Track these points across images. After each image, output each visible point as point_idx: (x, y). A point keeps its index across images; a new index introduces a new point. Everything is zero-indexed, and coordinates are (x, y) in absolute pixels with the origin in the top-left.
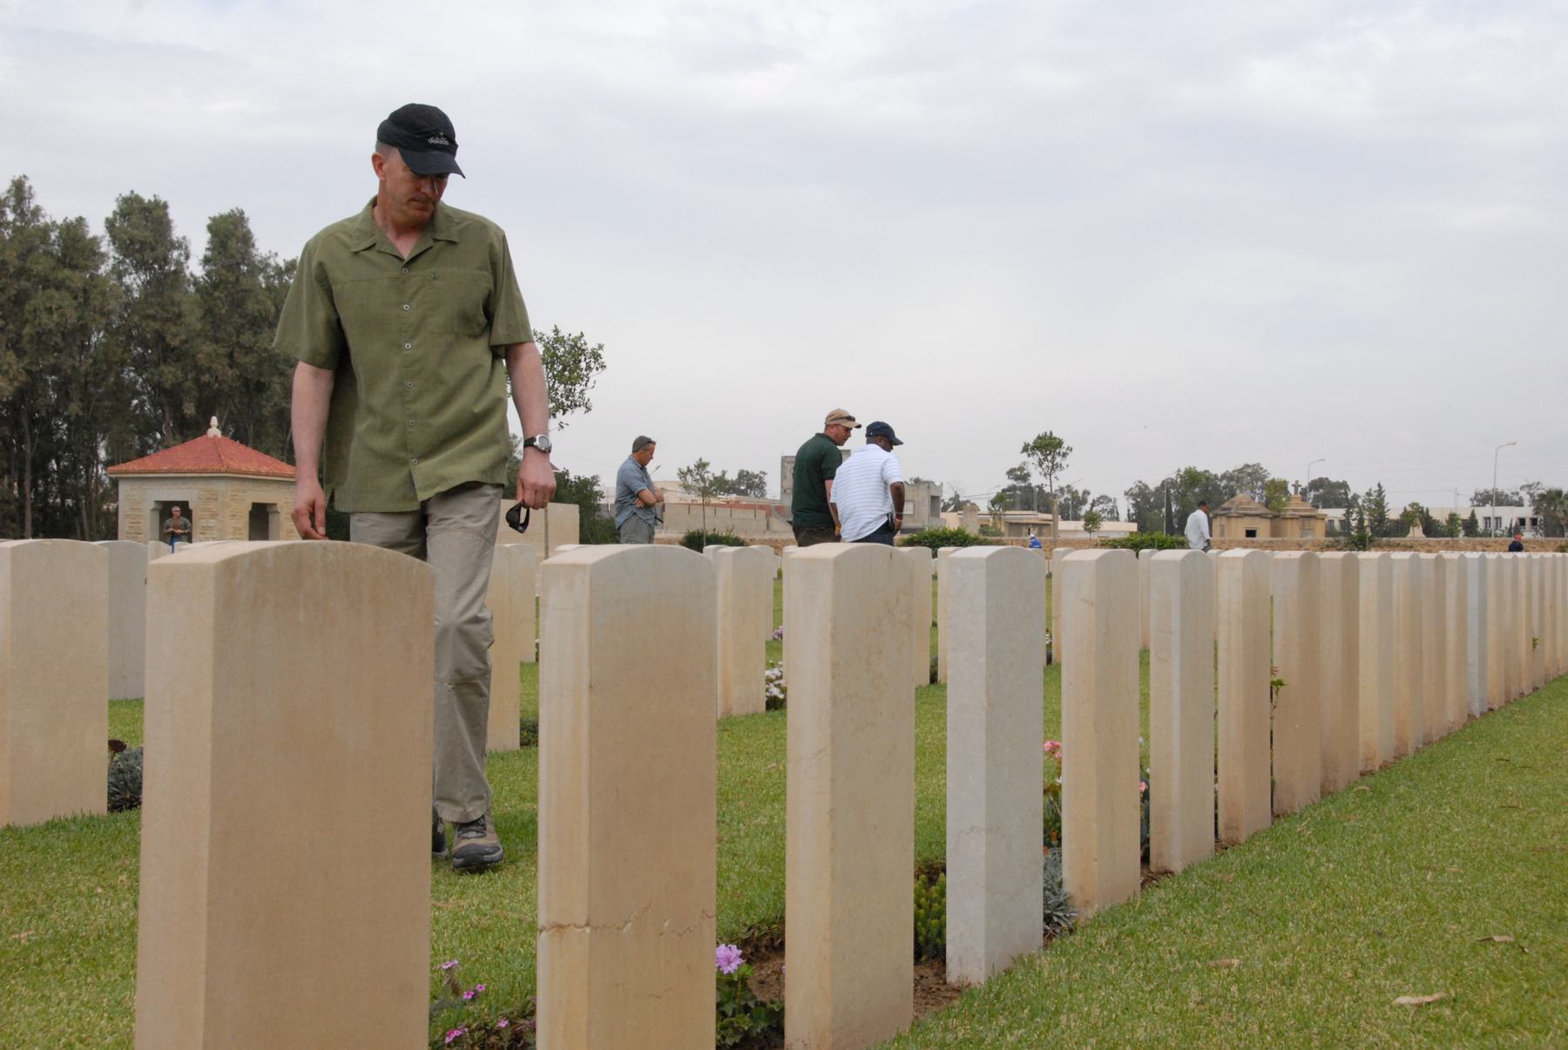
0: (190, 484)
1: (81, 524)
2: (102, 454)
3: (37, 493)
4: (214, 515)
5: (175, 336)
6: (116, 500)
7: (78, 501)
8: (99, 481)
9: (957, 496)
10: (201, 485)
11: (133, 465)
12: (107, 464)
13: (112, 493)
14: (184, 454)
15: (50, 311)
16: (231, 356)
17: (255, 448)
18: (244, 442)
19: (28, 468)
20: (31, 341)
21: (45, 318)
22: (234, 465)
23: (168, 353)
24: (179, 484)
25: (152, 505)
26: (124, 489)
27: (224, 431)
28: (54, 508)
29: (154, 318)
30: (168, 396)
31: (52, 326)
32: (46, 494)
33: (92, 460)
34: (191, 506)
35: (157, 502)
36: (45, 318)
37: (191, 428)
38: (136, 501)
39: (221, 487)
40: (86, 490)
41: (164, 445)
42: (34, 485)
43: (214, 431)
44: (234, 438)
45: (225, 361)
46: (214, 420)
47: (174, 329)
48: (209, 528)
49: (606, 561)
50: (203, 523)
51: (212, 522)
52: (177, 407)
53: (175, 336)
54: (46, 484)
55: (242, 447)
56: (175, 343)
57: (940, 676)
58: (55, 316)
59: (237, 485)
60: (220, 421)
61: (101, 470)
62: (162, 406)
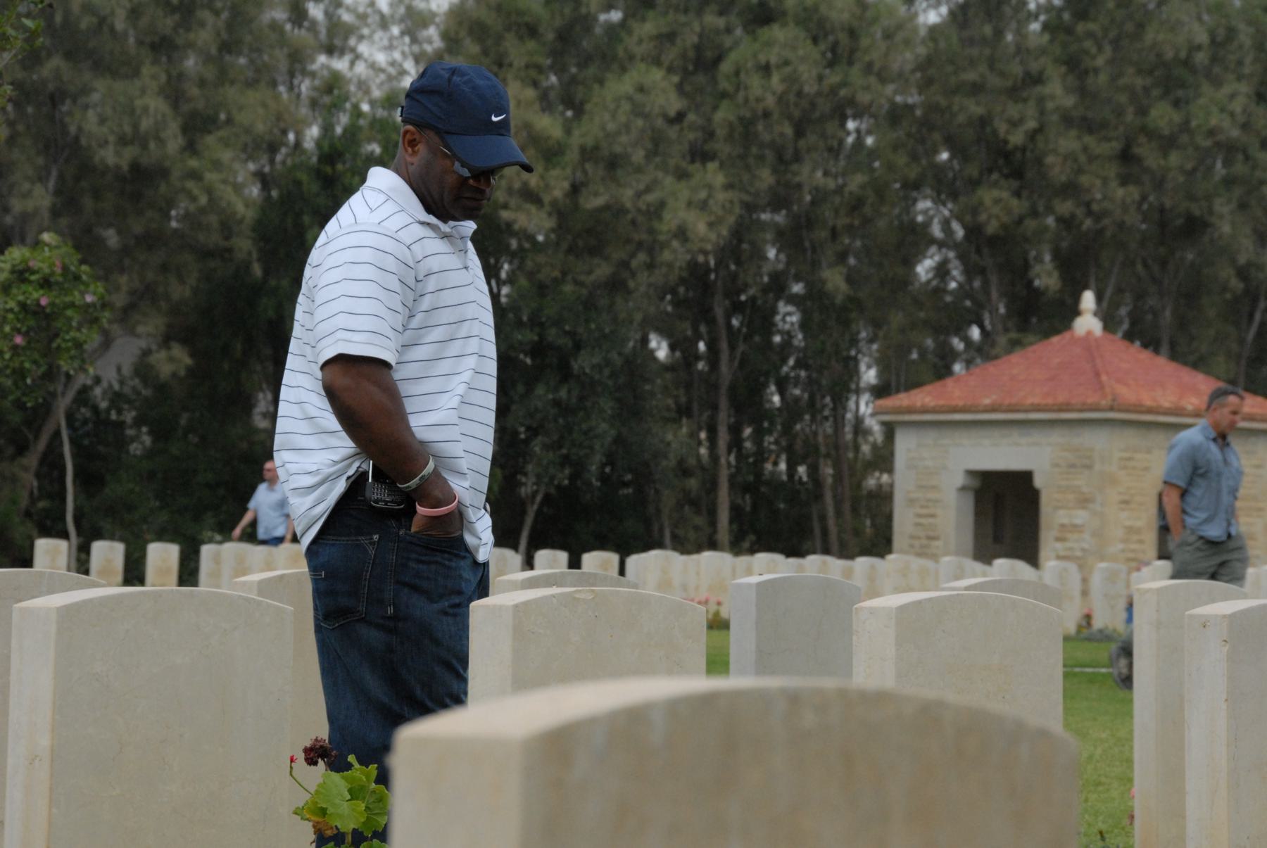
0: (1037, 436)
1: (823, 518)
2: (870, 375)
3: (740, 457)
4: (1084, 501)
5: (1014, 124)
6: (890, 470)
7: (814, 470)
8: (859, 428)
9: (314, 754)
10: (1057, 437)
11: (922, 397)
12: (880, 391)
13: (884, 459)
14: (1028, 371)
15: (766, 69)
16: (1126, 156)
17: (1175, 356)
18: (1152, 344)
19: (724, 403)
20: (730, 138)
21: (755, 83)
22: (1128, 394)
23: (1014, 165)
24: (1015, 435)
25: (960, 480)
26: (905, 445)
27: (1109, 322)
28: (775, 484)
29: (976, 89)
30: (992, 251)
31: (770, 101)
32: (761, 456)
33: (844, 386)
34: (1038, 482)
35: (971, 473)
36: (755, 83)
37: (1042, 316)
38: (931, 472)
39: (1097, 441)
40: (836, 445)
41: (983, 352)
42: (736, 443)
43: (1088, 322)
44: (1129, 336)
45: (1112, 170)
46: (1088, 300)
47: (1013, 110)
48: (1076, 528)
49: (1171, 586)
50: (1062, 517)
51: (1080, 516)
52: (1018, 272)
53: (1014, 124)
54: (759, 435)
55: (1146, 355)
56: (1017, 138)
57: (1189, 470)
58: (775, 79)
59: (1130, 438)
60: (1099, 298)
61: (864, 406)
62: (982, 271)
